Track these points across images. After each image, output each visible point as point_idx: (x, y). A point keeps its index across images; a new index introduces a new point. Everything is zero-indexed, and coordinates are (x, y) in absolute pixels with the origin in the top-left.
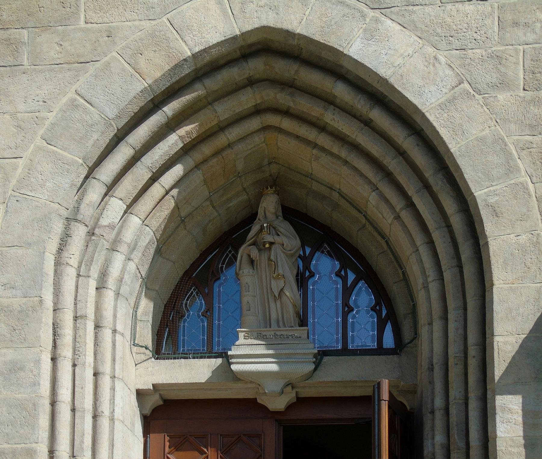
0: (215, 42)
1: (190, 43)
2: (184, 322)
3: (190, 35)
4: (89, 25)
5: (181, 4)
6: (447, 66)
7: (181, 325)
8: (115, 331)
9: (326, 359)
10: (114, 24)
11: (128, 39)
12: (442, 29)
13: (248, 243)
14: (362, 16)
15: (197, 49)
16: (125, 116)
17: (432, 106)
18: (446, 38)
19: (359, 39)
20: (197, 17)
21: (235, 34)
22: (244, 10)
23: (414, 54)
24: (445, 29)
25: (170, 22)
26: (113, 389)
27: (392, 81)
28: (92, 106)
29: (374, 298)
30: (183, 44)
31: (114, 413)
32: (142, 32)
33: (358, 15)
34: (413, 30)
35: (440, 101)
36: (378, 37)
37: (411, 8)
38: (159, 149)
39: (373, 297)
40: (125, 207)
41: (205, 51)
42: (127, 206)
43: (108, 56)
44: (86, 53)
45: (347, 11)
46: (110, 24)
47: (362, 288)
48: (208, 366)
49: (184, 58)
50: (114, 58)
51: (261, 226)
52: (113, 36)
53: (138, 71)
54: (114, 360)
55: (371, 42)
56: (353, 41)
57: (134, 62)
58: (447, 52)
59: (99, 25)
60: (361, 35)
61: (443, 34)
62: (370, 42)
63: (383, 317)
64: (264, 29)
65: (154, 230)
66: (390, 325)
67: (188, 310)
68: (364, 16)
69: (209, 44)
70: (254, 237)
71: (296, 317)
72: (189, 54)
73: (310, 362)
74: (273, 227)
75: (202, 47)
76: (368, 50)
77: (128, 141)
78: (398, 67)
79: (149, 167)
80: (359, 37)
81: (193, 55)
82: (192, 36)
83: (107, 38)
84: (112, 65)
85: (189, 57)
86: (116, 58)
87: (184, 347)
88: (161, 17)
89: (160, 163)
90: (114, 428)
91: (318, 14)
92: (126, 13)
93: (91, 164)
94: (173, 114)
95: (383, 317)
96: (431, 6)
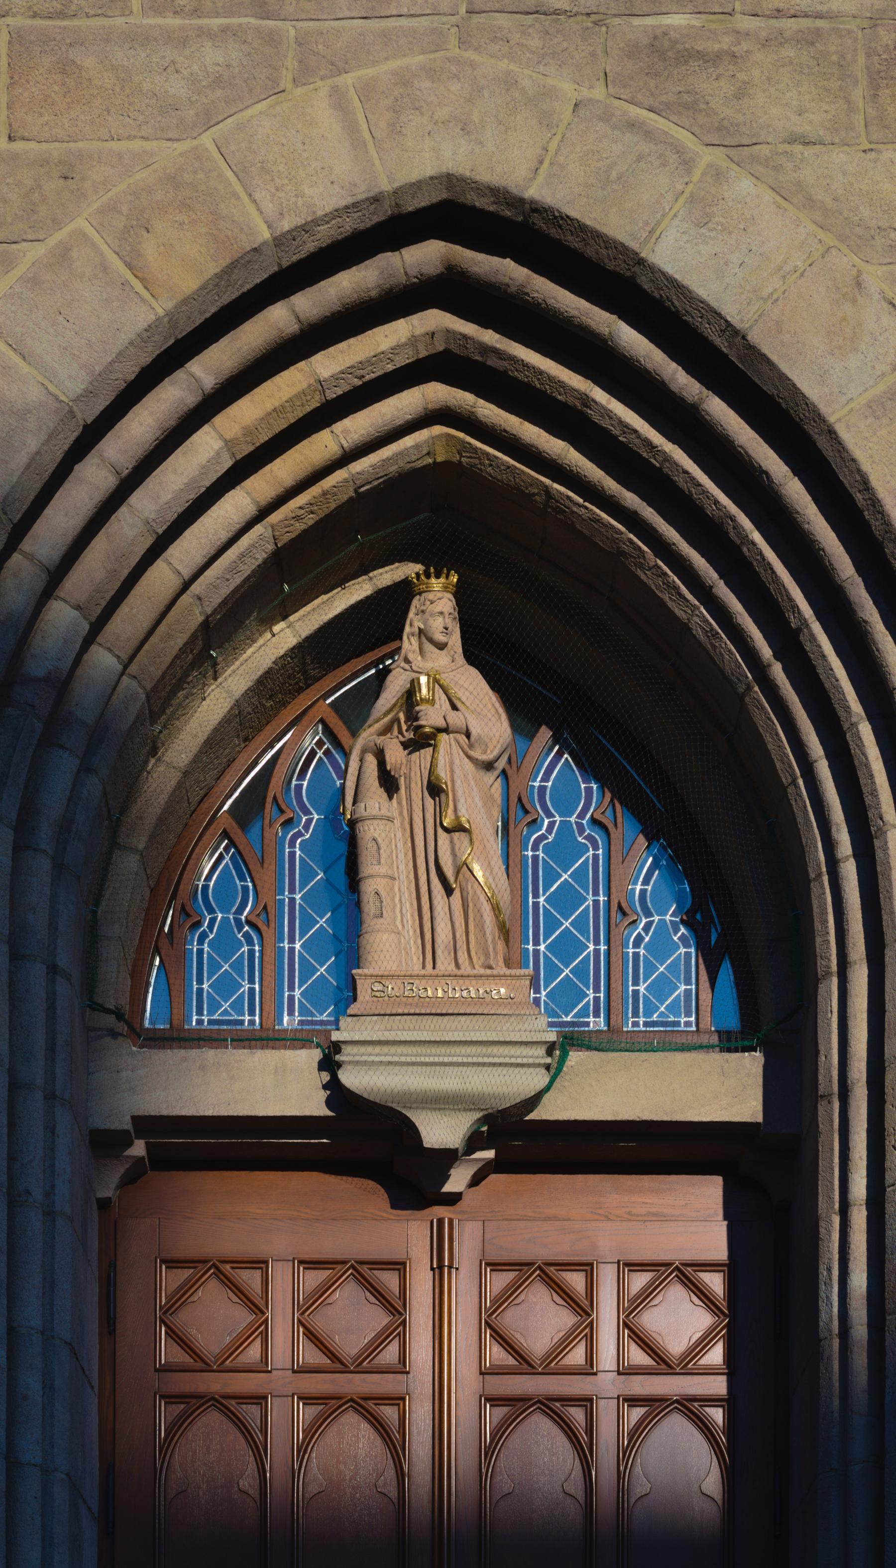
0: (328, 209)
1: (269, 208)
2: (201, 942)
3: (268, 187)
4: (18, 146)
5: (246, 104)
6: (885, 305)
7: (192, 949)
8: (53, 969)
9: (575, 1057)
10: (80, 145)
11: (114, 186)
12: (872, 208)
13: (377, 726)
14: (685, 162)
15: (286, 225)
16: (105, 392)
17: (851, 405)
18: (883, 233)
19: (676, 222)
20: (284, 141)
21: (377, 190)
22: (399, 129)
23: (808, 268)
24: (879, 210)
25: (218, 148)
26: (51, 1129)
27: (755, 337)
28: (24, 359)
29: (690, 888)
30: (252, 209)
31: (54, 1194)
32: (149, 170)
33: (673, 158)
34: (804, 206)
35: (869, 395)
36: (722, 219)
37: (797, 148)
38: (175, 471)
39: (687, 886)
40: (87, 627)
41: (305, 228)
42: (91, 624)
43: (64, 230)
44: (9, 219)
45: (645, 147)
46: (72, 145)
47: (660, 861)
48: (276, 1072)
49: (254, 246)
50: (81, 235)
51: (412, 682)
52: (77, 177)
53: (139, 274)
54: (51, 1048)
55: (704, 231)
56: (663, 226)
57: (128, 248)
58: (885, 268)
59: (44, 146)
60: (681, 212)
61: (874, 221)
62: (703, 230)
63: (713, 943)
64: (449, 179)
65: (148, 689)
66: (729, 966)
67: (211, 911)
68: (687, 164)
69: (314, 212)
70: (391, 710)
71: (499, 938)
72: (266, 234)
73: (539, 1065)
74: (442, 686)
75: (298, 219)
76: (699, 253)
77: (106, 455)
78: (770, 302)
79: (150, 521)
80: (675, 216)
81: (275, 239)
82: (273, 190)
83: (62, 181)
84: (74, 254)
85: (265, 243)
86: (84, 235)
87: (200, 1012)
88: (195, 135)
89: (174, 510)
90: (54, 1238)
91: (578, 149)
92: (110, 119)
93: (19, 516)
94: (216, 384)
95: (713, 943)
96: (846, 148)
